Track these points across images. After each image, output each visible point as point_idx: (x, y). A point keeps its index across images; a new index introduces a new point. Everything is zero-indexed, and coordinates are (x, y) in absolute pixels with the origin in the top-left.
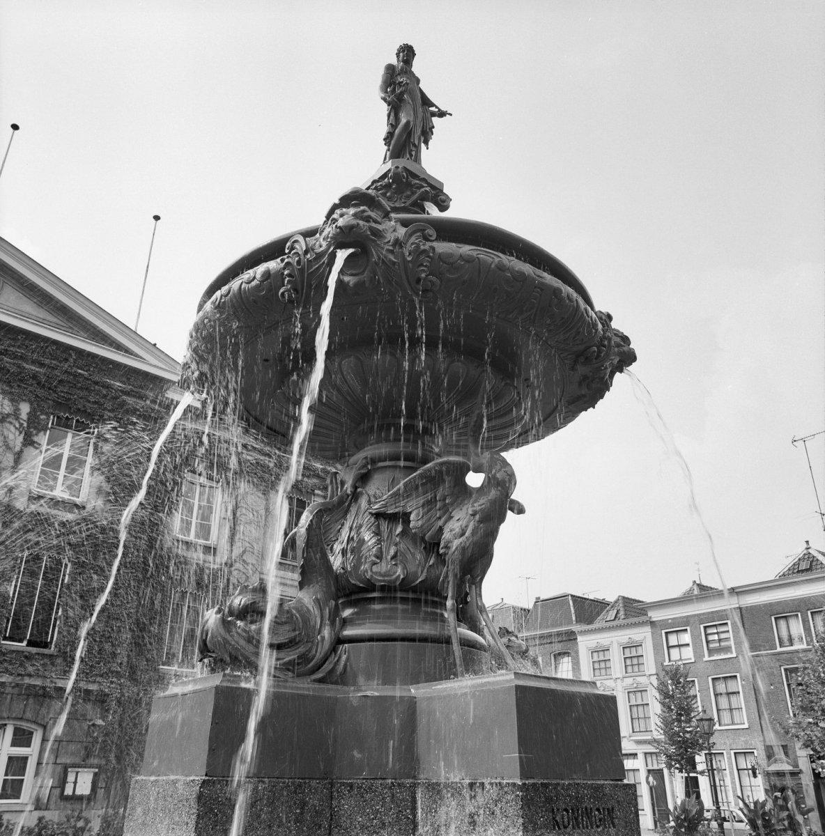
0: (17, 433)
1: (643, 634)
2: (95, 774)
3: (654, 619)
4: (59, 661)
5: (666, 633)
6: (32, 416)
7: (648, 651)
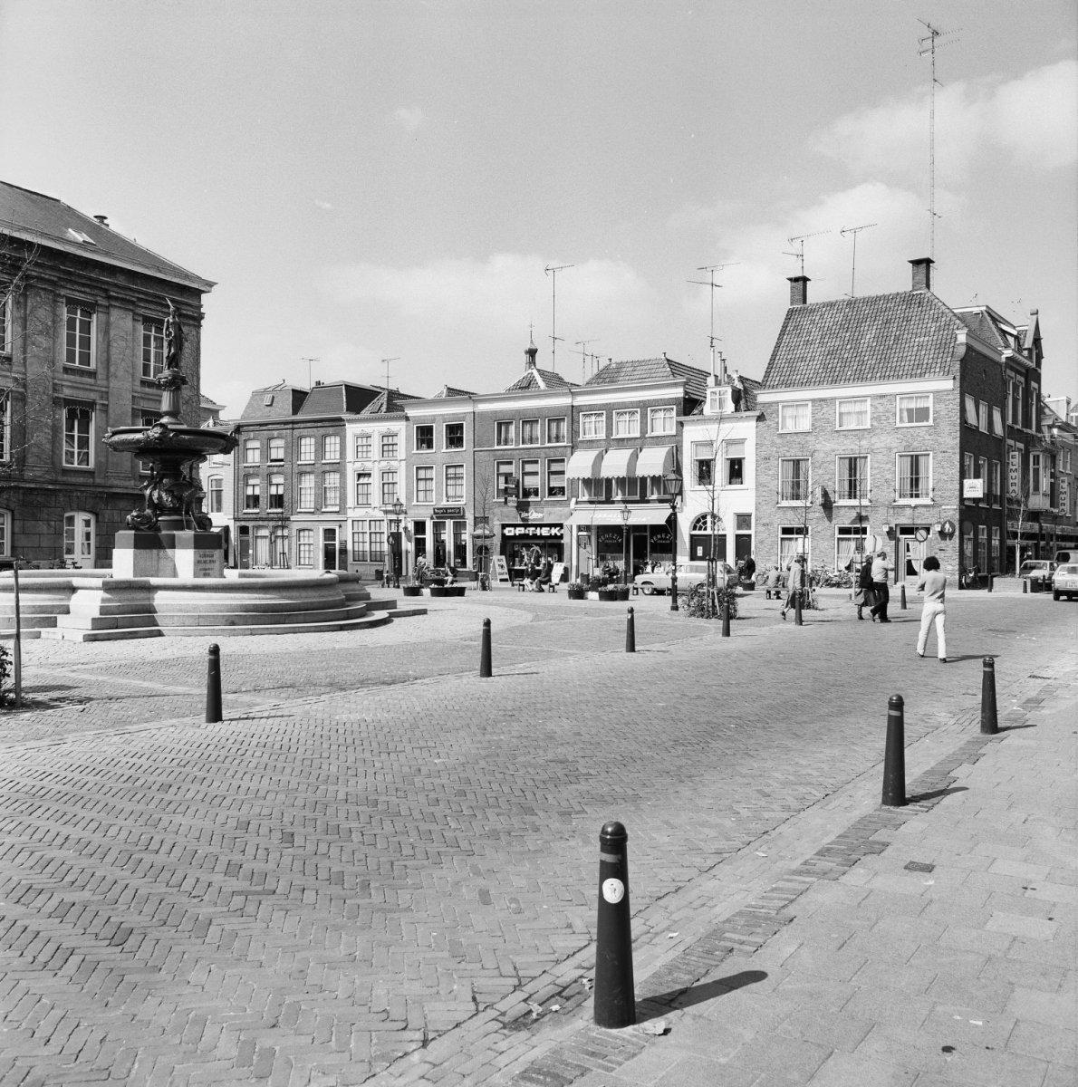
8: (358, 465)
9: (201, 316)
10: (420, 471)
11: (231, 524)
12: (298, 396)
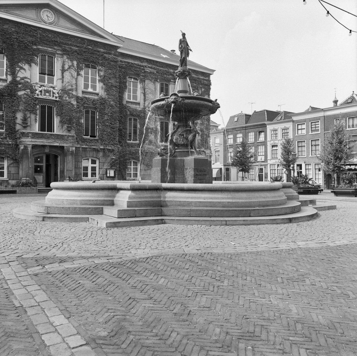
0: (75, 72)
1: (290, 125)
2: (114, 171)
3: (294, 120)
4: (99, 141)
5: (298, 125)
6: (78, 64)
7: (291, 131)
8: (272, 142)
9: (210, 84)
10: (299, 143)
11: (223, 167)
12: (247, 117)
